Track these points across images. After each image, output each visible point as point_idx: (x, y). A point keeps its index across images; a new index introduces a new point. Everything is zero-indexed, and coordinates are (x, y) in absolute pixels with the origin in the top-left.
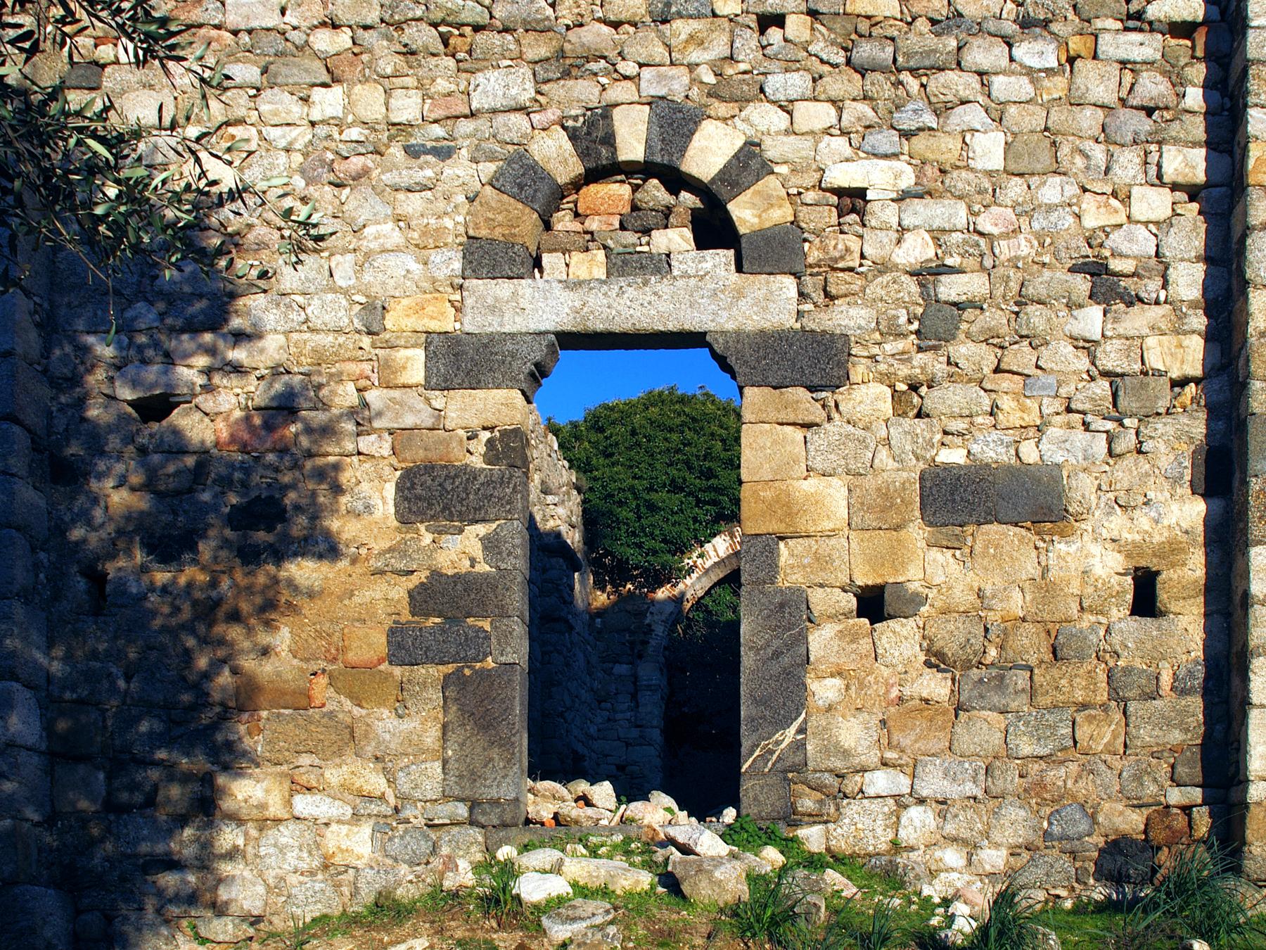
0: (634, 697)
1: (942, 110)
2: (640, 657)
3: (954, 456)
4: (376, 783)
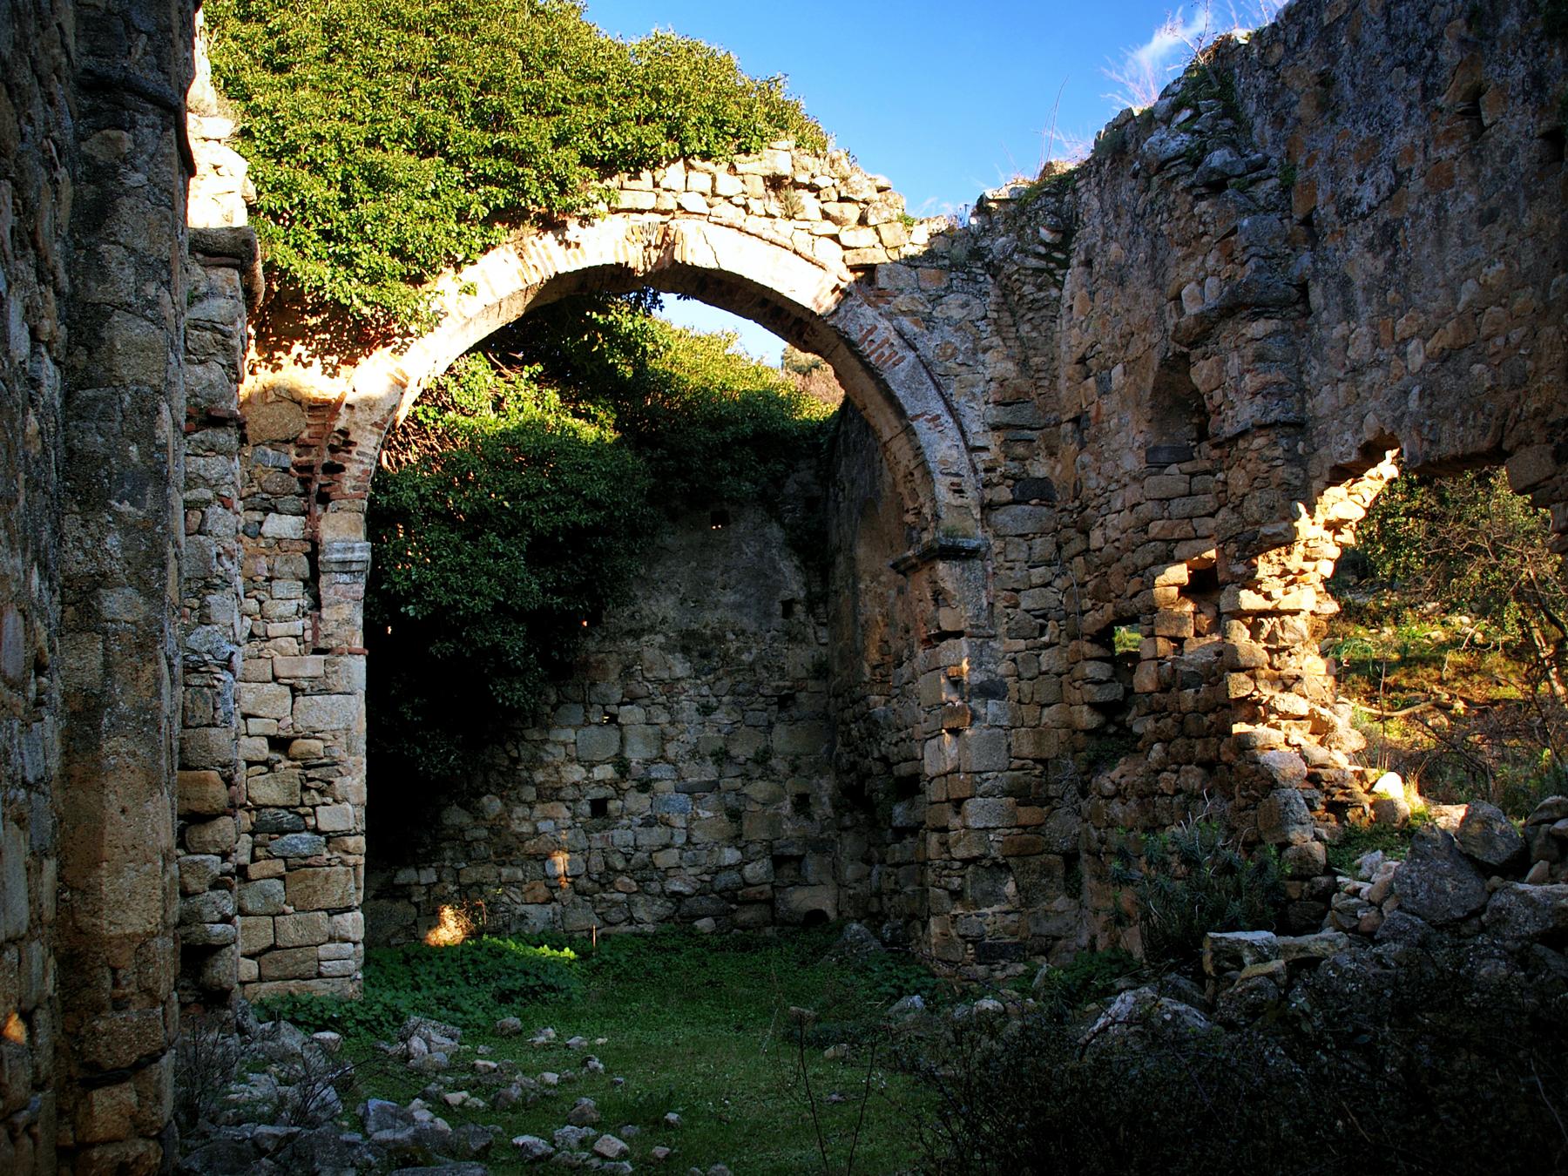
0: (311, 583)
2: (324, 499)
3: (1327, 569)
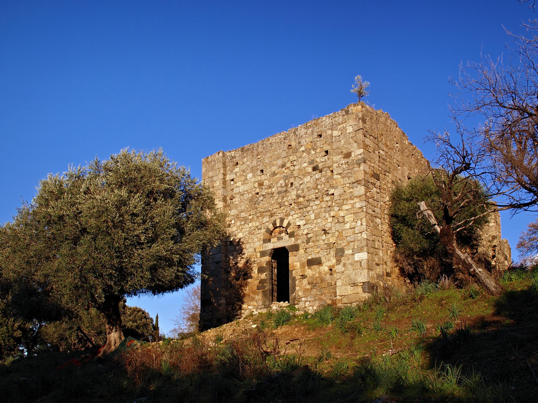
1: (308, 212)
3: (310, 258)
4: (256, 304)
